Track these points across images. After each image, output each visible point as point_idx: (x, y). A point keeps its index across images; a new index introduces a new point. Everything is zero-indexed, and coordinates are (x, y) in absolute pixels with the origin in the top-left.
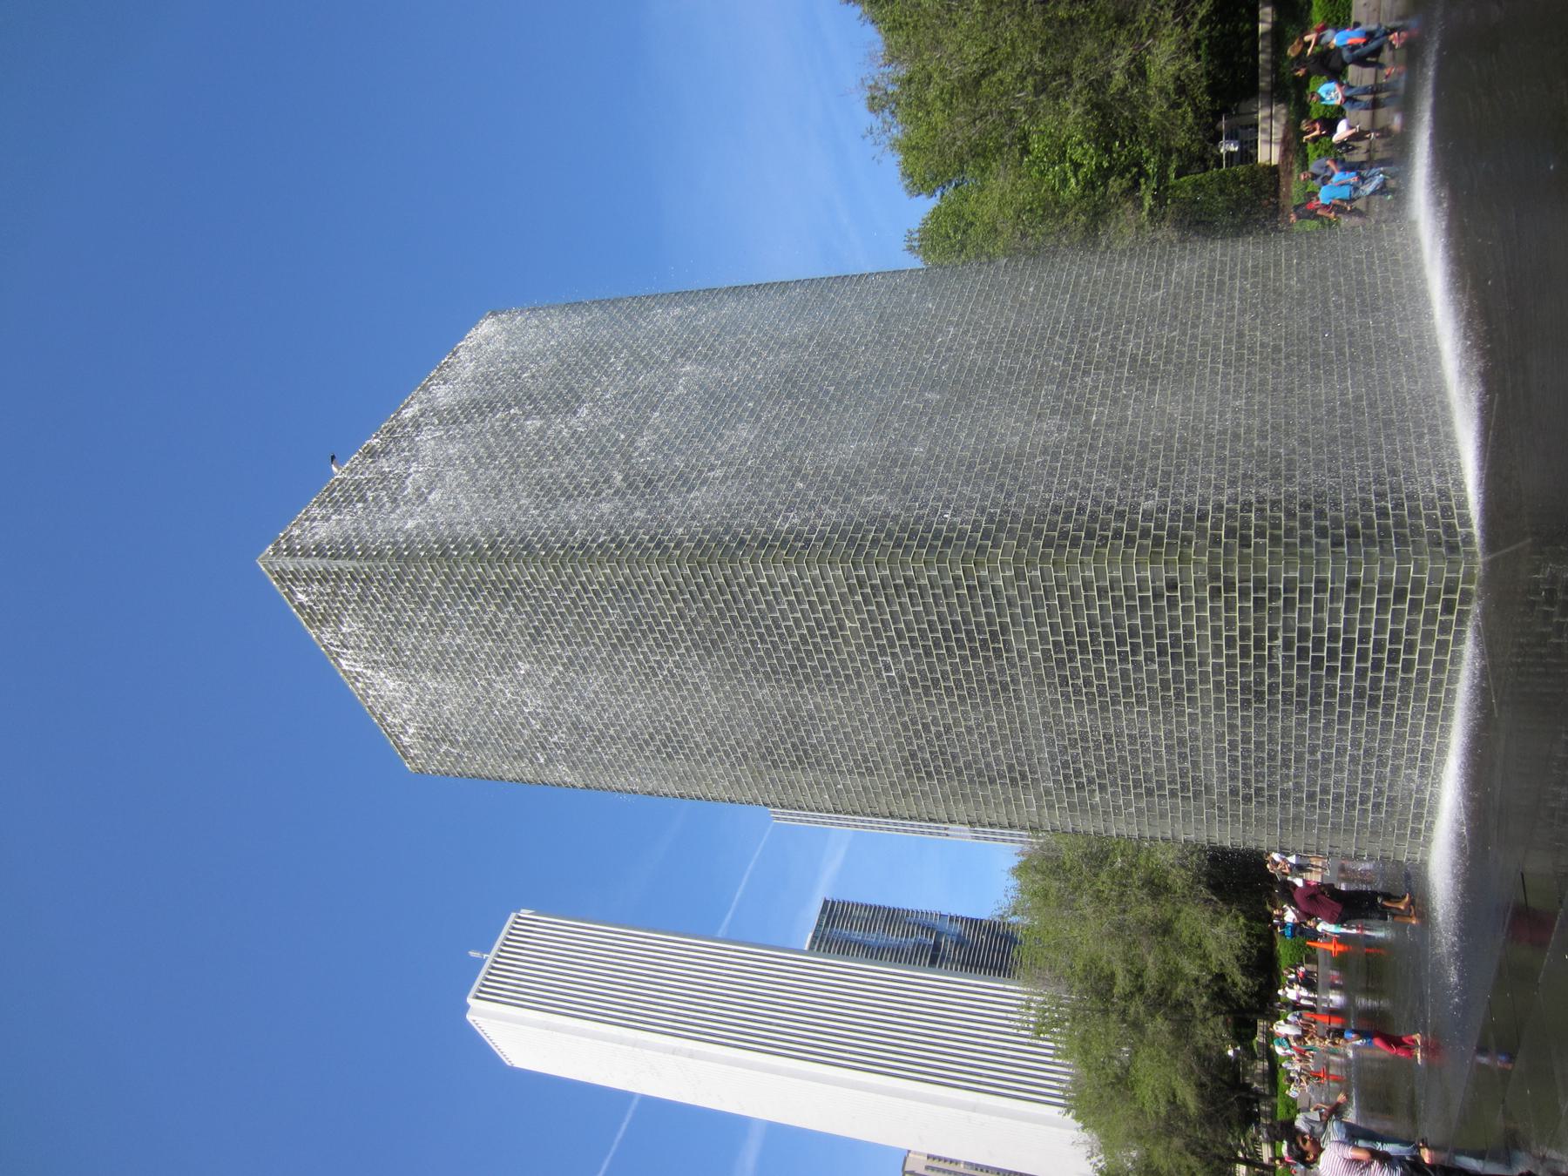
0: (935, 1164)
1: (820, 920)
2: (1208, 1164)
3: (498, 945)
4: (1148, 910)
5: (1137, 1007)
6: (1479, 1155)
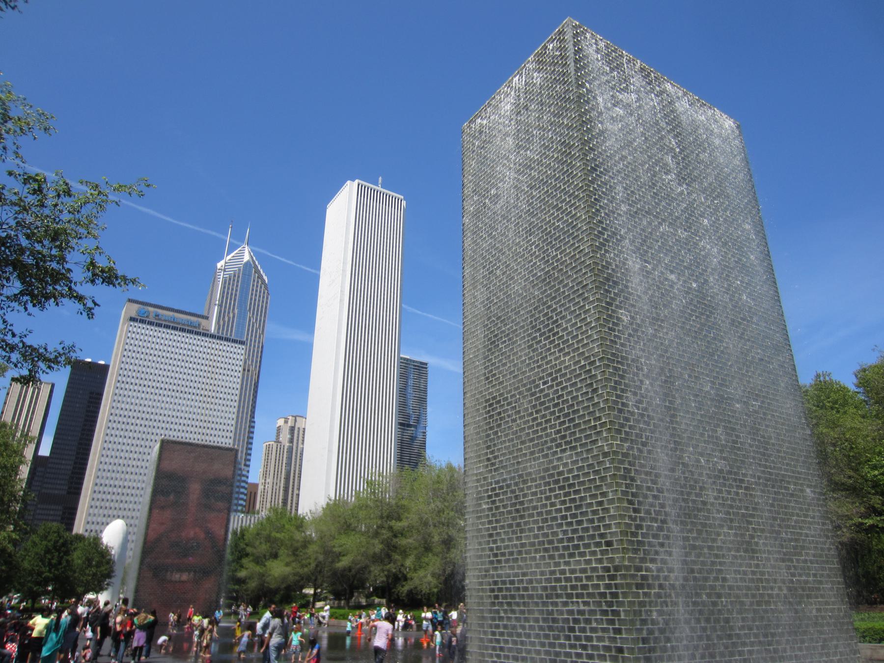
0: (301, 432)
1: (416, 362)
2: (312, 574)
3: (386, 191)
4: (436, 538)
5: (386, 534)
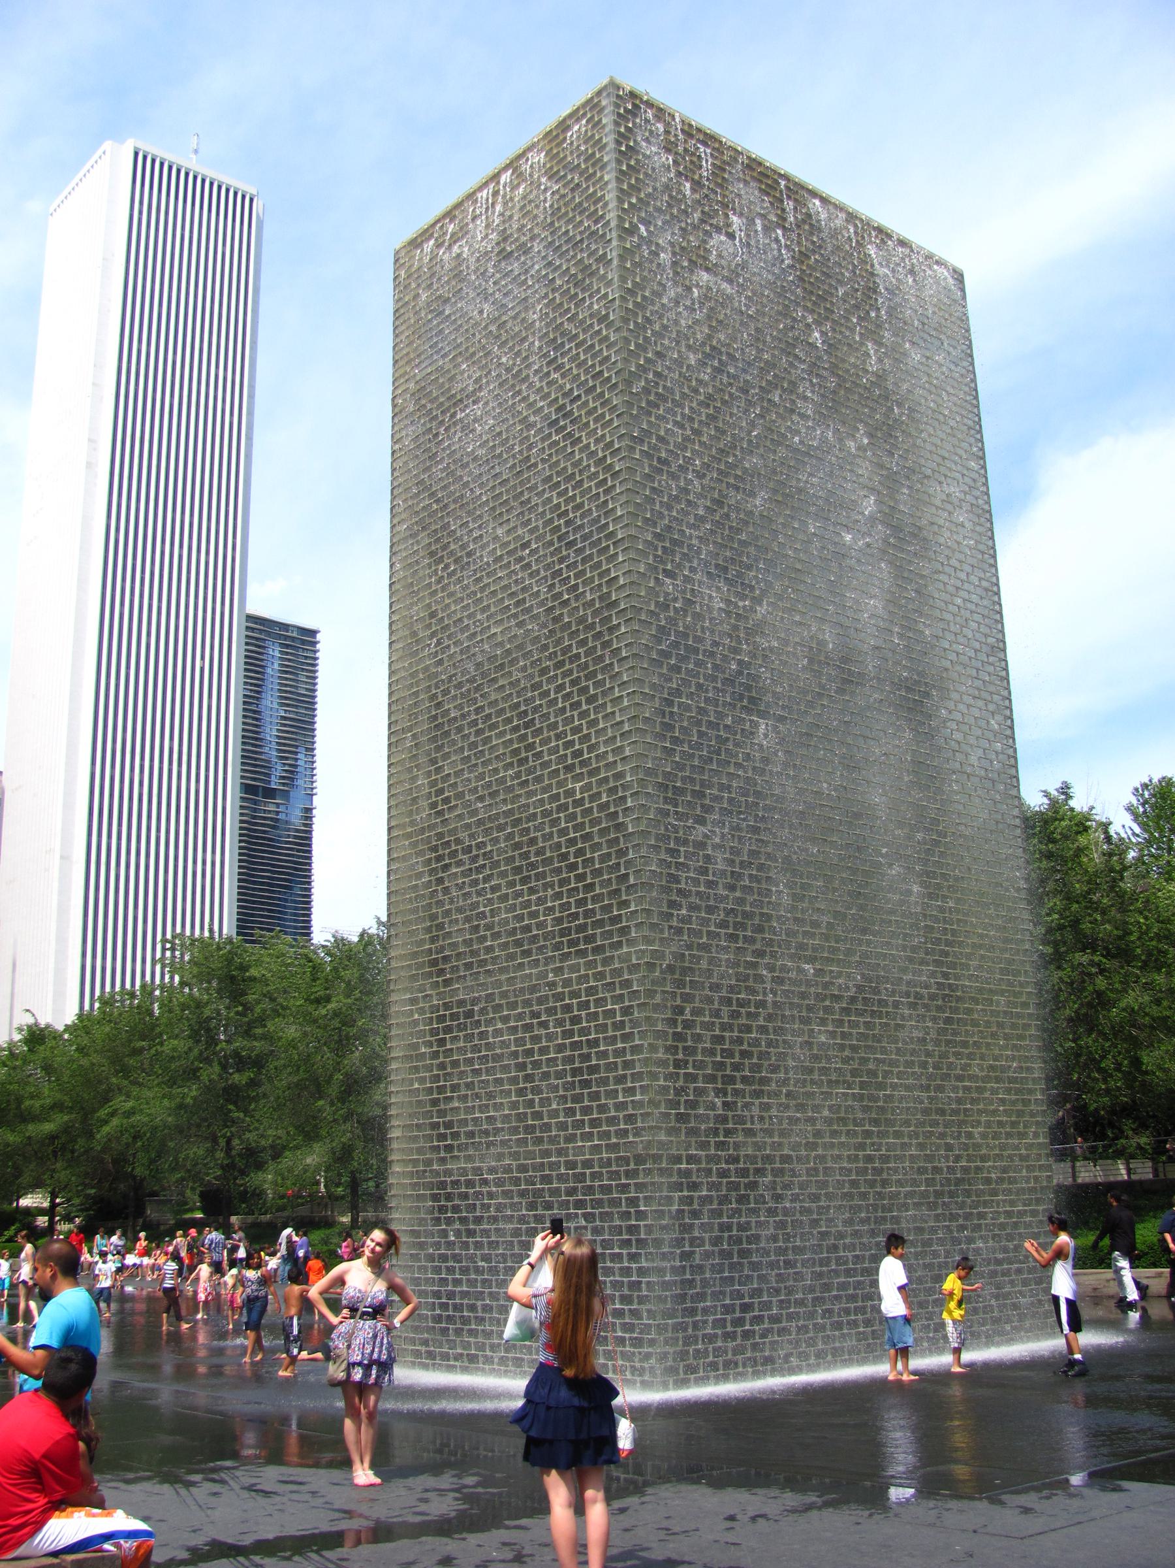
6: (54, 1464)
